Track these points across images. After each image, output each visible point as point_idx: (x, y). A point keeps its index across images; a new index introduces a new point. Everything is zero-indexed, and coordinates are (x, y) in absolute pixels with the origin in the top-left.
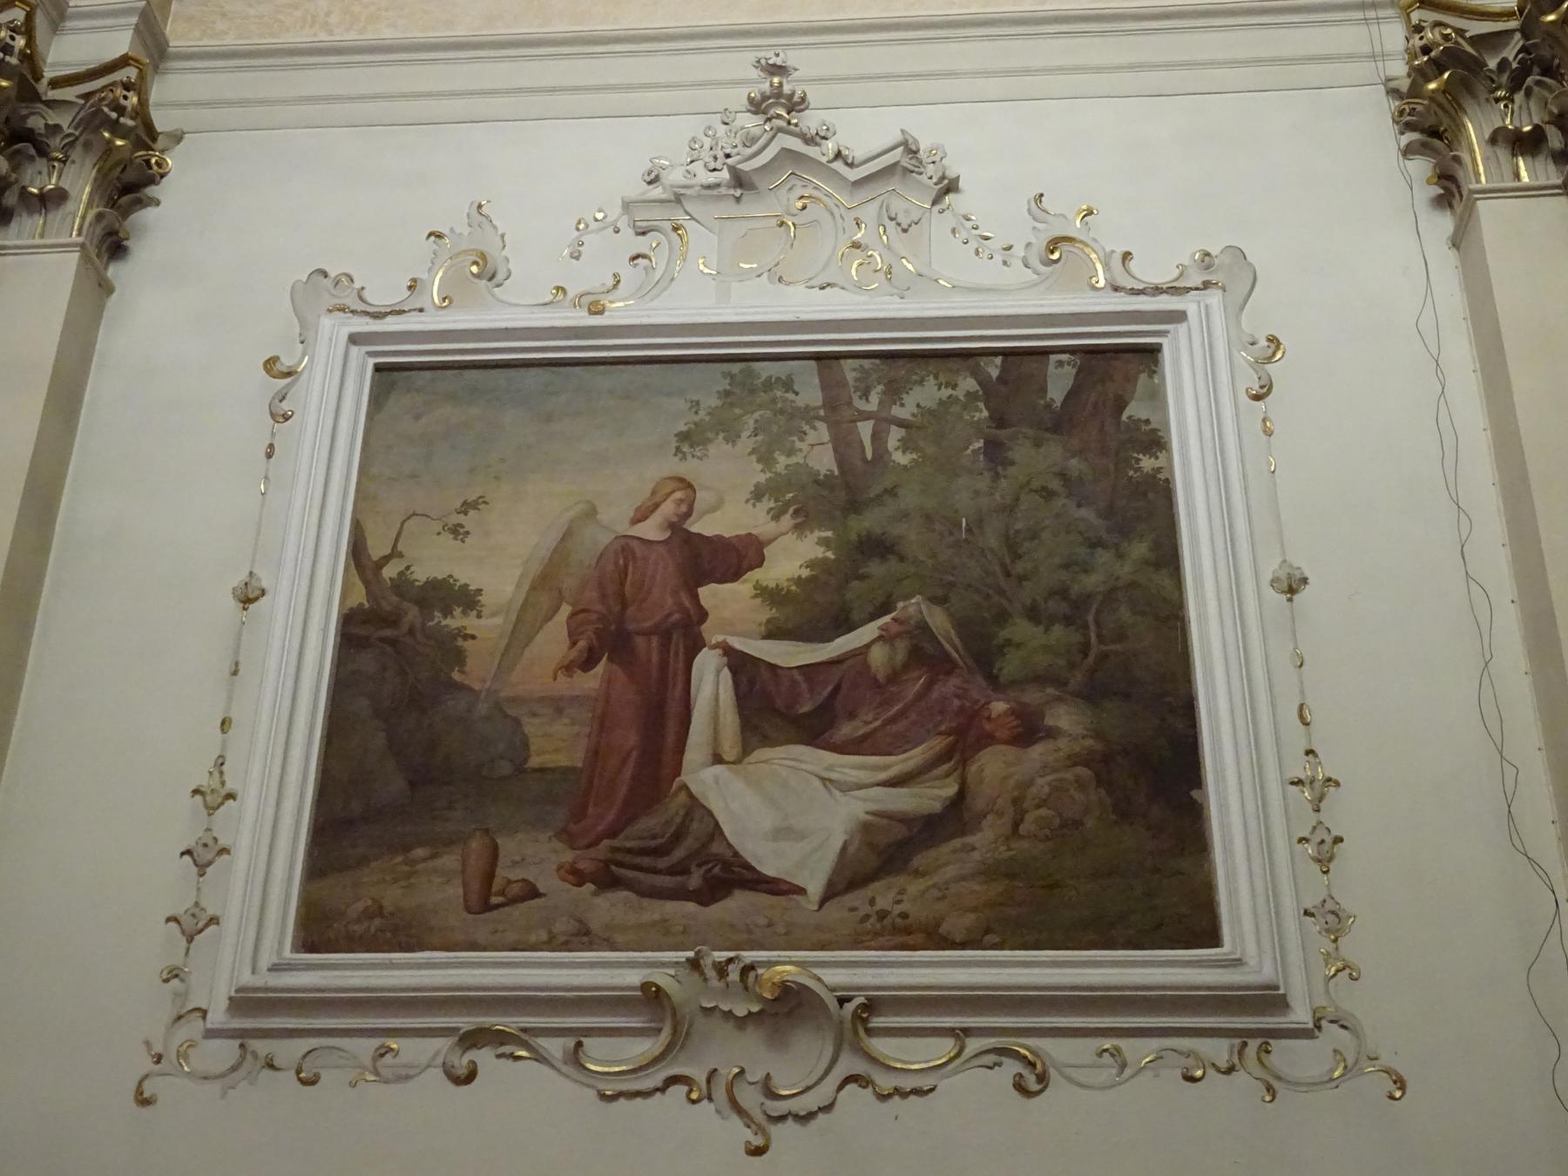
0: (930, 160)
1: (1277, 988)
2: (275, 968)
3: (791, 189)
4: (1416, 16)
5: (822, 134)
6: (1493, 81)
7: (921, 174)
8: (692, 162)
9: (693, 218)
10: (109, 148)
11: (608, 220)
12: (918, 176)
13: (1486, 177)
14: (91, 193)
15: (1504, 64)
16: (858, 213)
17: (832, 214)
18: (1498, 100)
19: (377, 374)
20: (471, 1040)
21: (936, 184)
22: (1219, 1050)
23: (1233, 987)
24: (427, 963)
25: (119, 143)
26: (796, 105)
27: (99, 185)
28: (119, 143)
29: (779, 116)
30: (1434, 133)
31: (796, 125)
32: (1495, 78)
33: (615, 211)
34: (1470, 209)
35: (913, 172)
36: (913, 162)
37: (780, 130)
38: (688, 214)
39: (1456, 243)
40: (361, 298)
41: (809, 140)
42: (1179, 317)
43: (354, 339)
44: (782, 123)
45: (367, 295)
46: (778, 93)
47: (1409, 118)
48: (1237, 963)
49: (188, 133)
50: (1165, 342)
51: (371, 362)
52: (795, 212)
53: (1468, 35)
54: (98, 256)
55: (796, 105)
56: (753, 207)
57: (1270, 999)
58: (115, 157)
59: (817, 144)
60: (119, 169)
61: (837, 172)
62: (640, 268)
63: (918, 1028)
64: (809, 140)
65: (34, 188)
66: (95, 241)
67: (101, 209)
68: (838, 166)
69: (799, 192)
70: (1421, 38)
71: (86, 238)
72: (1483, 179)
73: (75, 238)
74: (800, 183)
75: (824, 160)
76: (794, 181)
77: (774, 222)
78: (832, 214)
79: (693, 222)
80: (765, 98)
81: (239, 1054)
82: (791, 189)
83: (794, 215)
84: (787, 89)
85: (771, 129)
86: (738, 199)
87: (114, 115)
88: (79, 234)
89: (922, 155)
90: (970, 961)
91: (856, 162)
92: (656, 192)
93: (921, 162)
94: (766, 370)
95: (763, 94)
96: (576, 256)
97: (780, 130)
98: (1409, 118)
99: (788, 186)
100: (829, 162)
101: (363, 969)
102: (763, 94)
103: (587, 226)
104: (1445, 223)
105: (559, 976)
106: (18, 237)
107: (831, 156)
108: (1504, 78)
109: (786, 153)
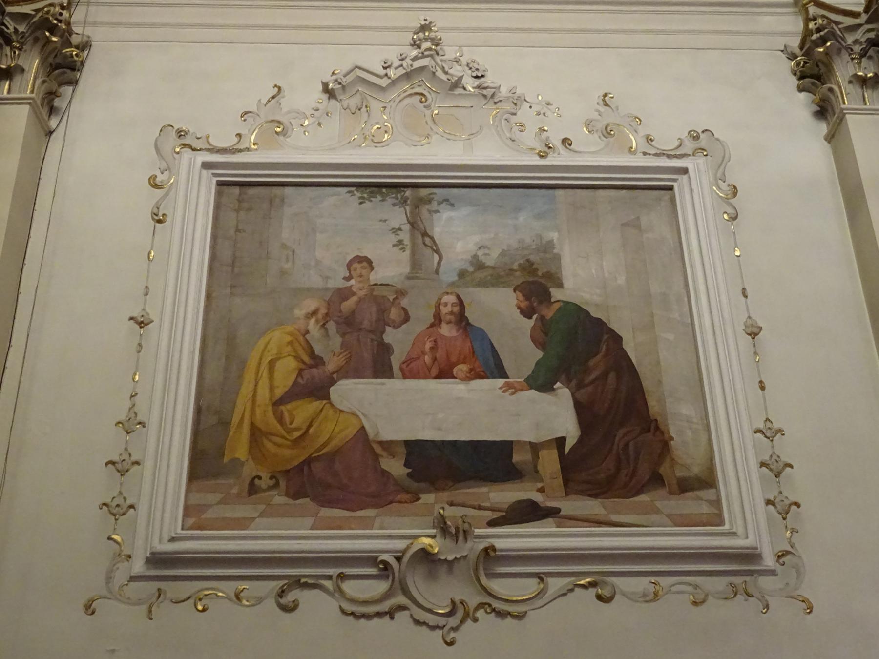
1: (756, 548)
2: (173, 540)
10: (48, 41)
13: (848, 102)
14: (38, 65)
15: (856, 42)
19: (218, 187)
20: (298, 583)
22: (719, 584)
23: (225, 552)
24: (516, 535)
25: (54, 39)
27: (43, 62)
30: (818, 77)
34: (842, 119)
39: (830, 138)
40: (208, 143)
42: (685, 171)
43: (206, 166)
45: (211, 140)
47: (801, 69)
48: (734, 534)
50: (675, 185)
51: (215, 180)
54: (42, 105)
57: (751, 556)
58: (53, 46)
60: (53, 55)
63: (364, 575)
65: (3, 65)
66: (41, 96)
67: (45, 78)
70: (816, 24)
71: (36, 94)
72: (868, 103)
73: (28, 94)
87: (55, 22)
88: (32, 92)
90: (621, 534)
94: (424, 192)
98: (801, 69)
104: (823, 128)
105: (208, 544)
106: (20, 92)
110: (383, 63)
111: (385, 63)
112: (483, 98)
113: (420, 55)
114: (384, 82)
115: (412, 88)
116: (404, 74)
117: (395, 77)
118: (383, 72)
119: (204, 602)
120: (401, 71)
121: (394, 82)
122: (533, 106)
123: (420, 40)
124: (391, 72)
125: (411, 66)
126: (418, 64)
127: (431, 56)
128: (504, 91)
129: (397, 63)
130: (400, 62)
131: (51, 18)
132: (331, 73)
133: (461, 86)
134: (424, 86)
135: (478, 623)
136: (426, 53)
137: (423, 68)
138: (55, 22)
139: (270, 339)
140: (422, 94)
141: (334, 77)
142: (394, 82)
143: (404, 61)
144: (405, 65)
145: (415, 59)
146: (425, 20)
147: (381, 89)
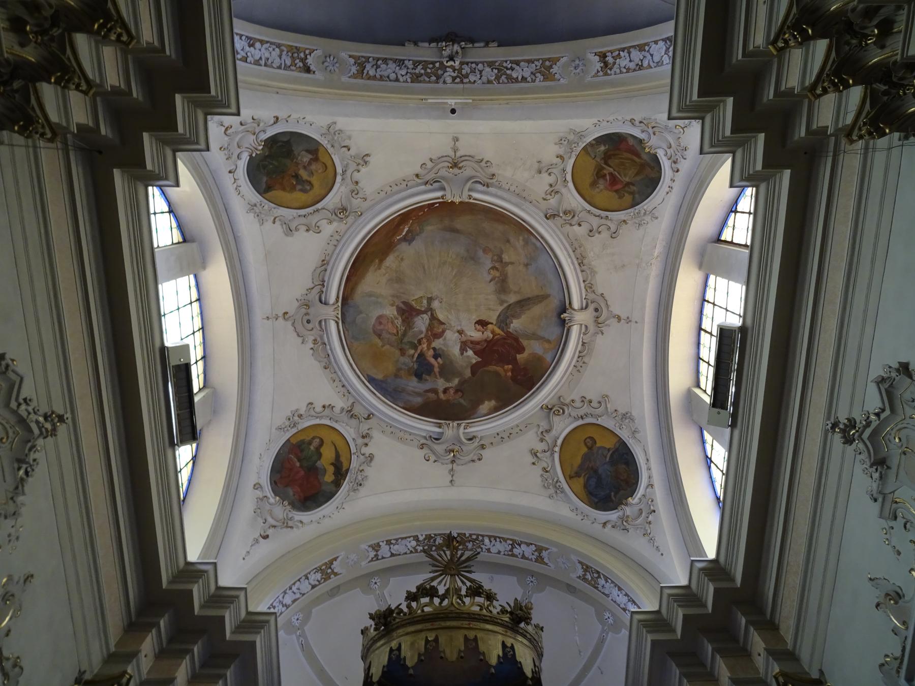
0: (889, 373)
3: (890, 441)
4: (855, 138)
5: (866, 418)
6: (895, 97)
7: (894, 379)
8: (872, 477)
9: (893, 492)
11: (887, 529)
12: (895, 381)
16: (908, 415)
17: (905, 428)
18: (905, 94)
21: (900, 375)
25: (96, 26)
26: (852, 423)
28: (96, 26)
29: (854, 434)
31: (859, 428)
32: (892, 96)
33: (884, 523)
35: (892, 384)
36: (887, 381)
37: (860, 436)
38: (890, 493)
41: (868, 424)
44: (857, 434)
46: (843, 431)
49: (16, 145)
52: (900, 444)
53: (870, 111)
55: (852, 423)
56: (894, 462)
59: (871, 422)
61: (885, 418)
62: (911, 528)
64: (868, 424)
68: (883, 416)
69: (892, 438)
74: (888, 436)
75: (878, 422)
76: (887, 438)
77: (903, 456)
78: (905, 428)
79: (896, 492)
80: (844, 437)
81: (805, 655)
82: (890, 441)
83: (902, 446)
84: (841, 426)
85: (858, 440)
86: (889, 468)
87: (109, 26)
89: (885, 375)
91: (882, 407)
92: (880, 500)
93: (889, 378)
95: (842, 438)
96: (899, 553)
97: (860, 436)
99: (888, 442)
100: (879, 420)
101: (380, 409)
102: (842, 438)
103: (887, 539)
107: (877, 418)
108: (893, 91)
109: (871, 437)
110: (28, 398)
111: (30, 400)
112: (14, 487)
113: (41, 425)
114: (13, 405)
115: (11, 427)
116: (22, 417)
117: (20, 412)
118: (21, 401)
119: (903, 433)
120: (24, 414)
121: (15, 412)
122: (14, 529)
123: (52, 420)
124: (23, 407)
125: (32, 421)
126: (34, 427)
127: (41, 433)
128: (21, 499)
129: (30, 409)
130: (31, 411)
131: (69, 75)
132: (12, 358)
133: (21, 465)
134: (14, 436)
135: (549, 177)
136: (43, 430)
137: (30, 431)
138: (109, 26)
139: (370, 662)
140: (8, 437)
141: (10, 362)
142: (15, 412)
143: (33, 414)
144: (31, 416)
145: (37, 422)
146: (67, 419)
147: (7, 405)
